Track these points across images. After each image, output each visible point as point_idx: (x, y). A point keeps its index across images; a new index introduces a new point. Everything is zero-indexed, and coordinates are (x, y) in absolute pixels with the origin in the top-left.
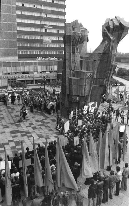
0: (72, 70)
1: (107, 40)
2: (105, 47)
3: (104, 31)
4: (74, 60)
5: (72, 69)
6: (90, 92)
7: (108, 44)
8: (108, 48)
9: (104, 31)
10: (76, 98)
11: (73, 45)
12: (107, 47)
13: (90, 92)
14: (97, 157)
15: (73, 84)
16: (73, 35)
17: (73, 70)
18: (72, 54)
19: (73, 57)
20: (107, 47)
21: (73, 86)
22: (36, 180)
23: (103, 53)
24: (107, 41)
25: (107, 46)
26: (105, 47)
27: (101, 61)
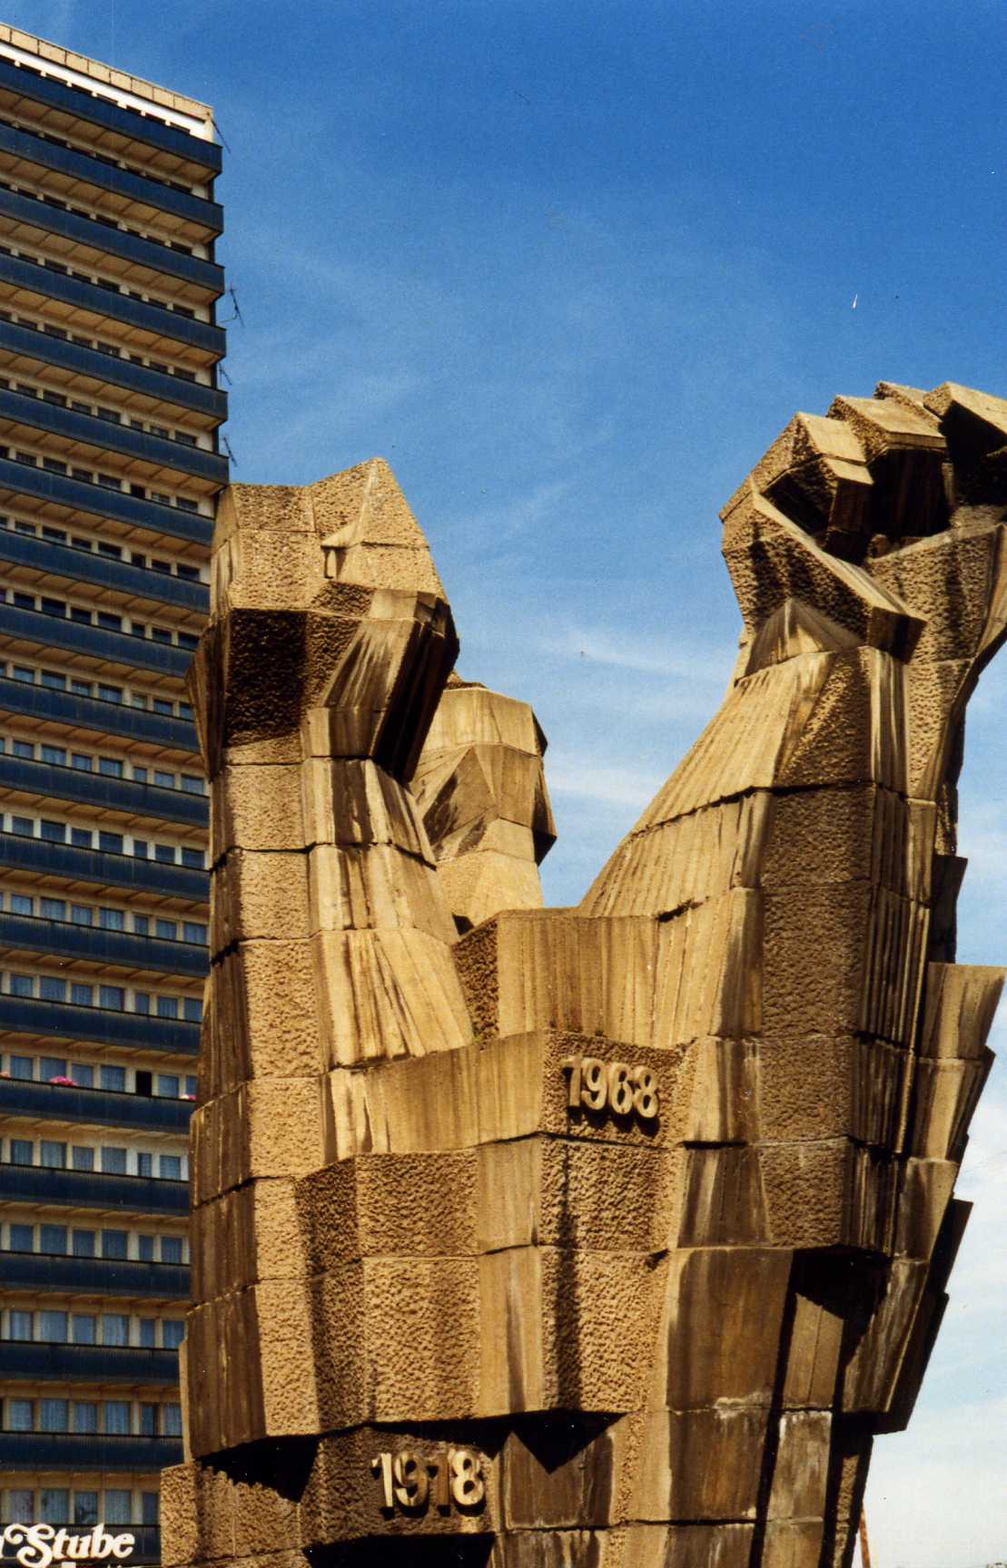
0: (333, 1066)
1: (810, 632)
2: (793, 713)
3: (757, 536)
4: (358, 940)
5: (345, 1055)
6: (609, 983)
7: (827, 671)
8: (834, 714)
9: (757, 536)
10: (432, 1471)
11: (337, 756)
12: (817, 702)
13: (609, 983)
14: (659, 803)
15: (367, 1242)
16: (327, 612)
17: (359, 1066)
18: (327, 859)
19: (347, 893)
20: (824, 713)
21: (379, 1269)
22: (126, 1049)
23: (776, 792)
24: (807, 643)
25: (822, 690)
26: (805, 709)
27: (760, 902)
